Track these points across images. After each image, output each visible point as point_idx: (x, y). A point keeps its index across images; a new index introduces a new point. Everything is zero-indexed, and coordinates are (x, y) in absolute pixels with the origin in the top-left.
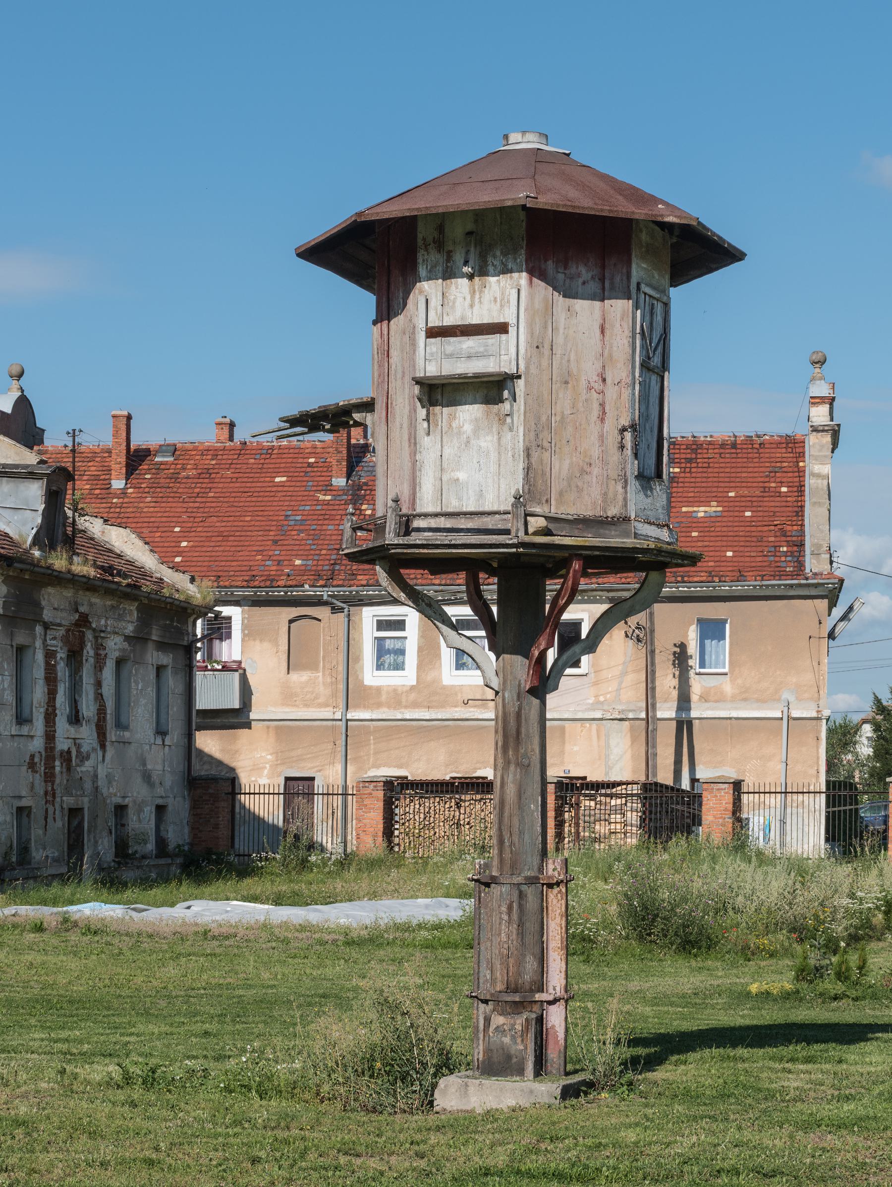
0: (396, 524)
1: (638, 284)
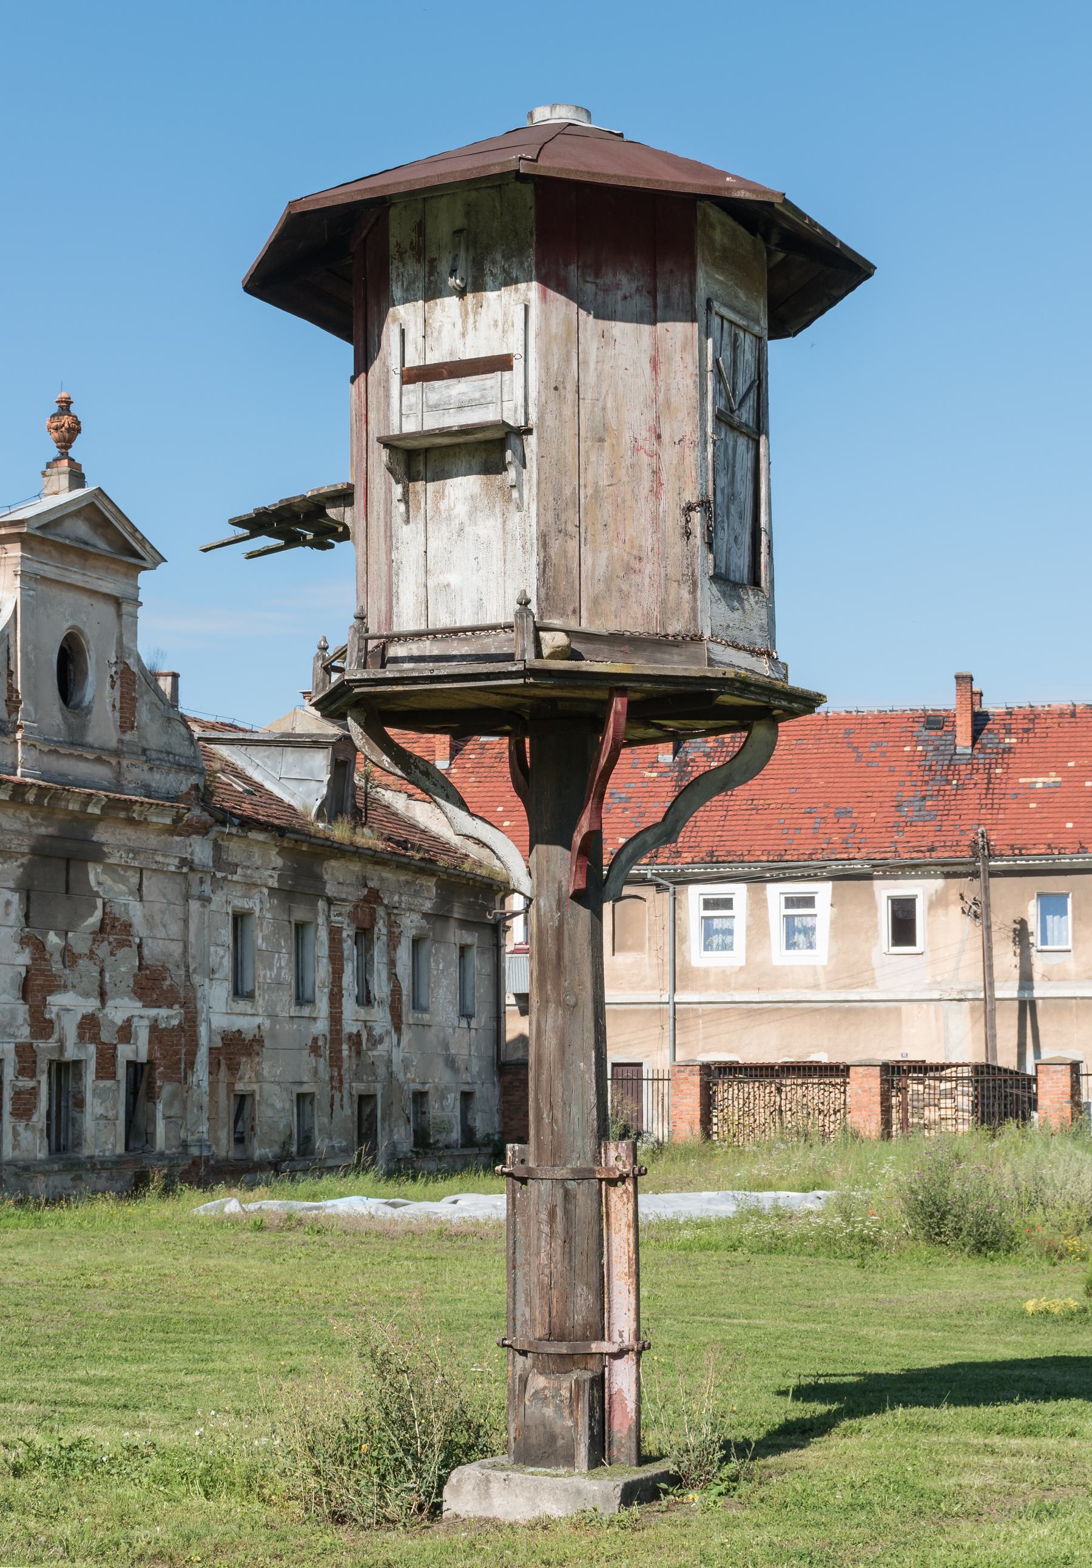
0: (360, 650)
1: (709, 301)
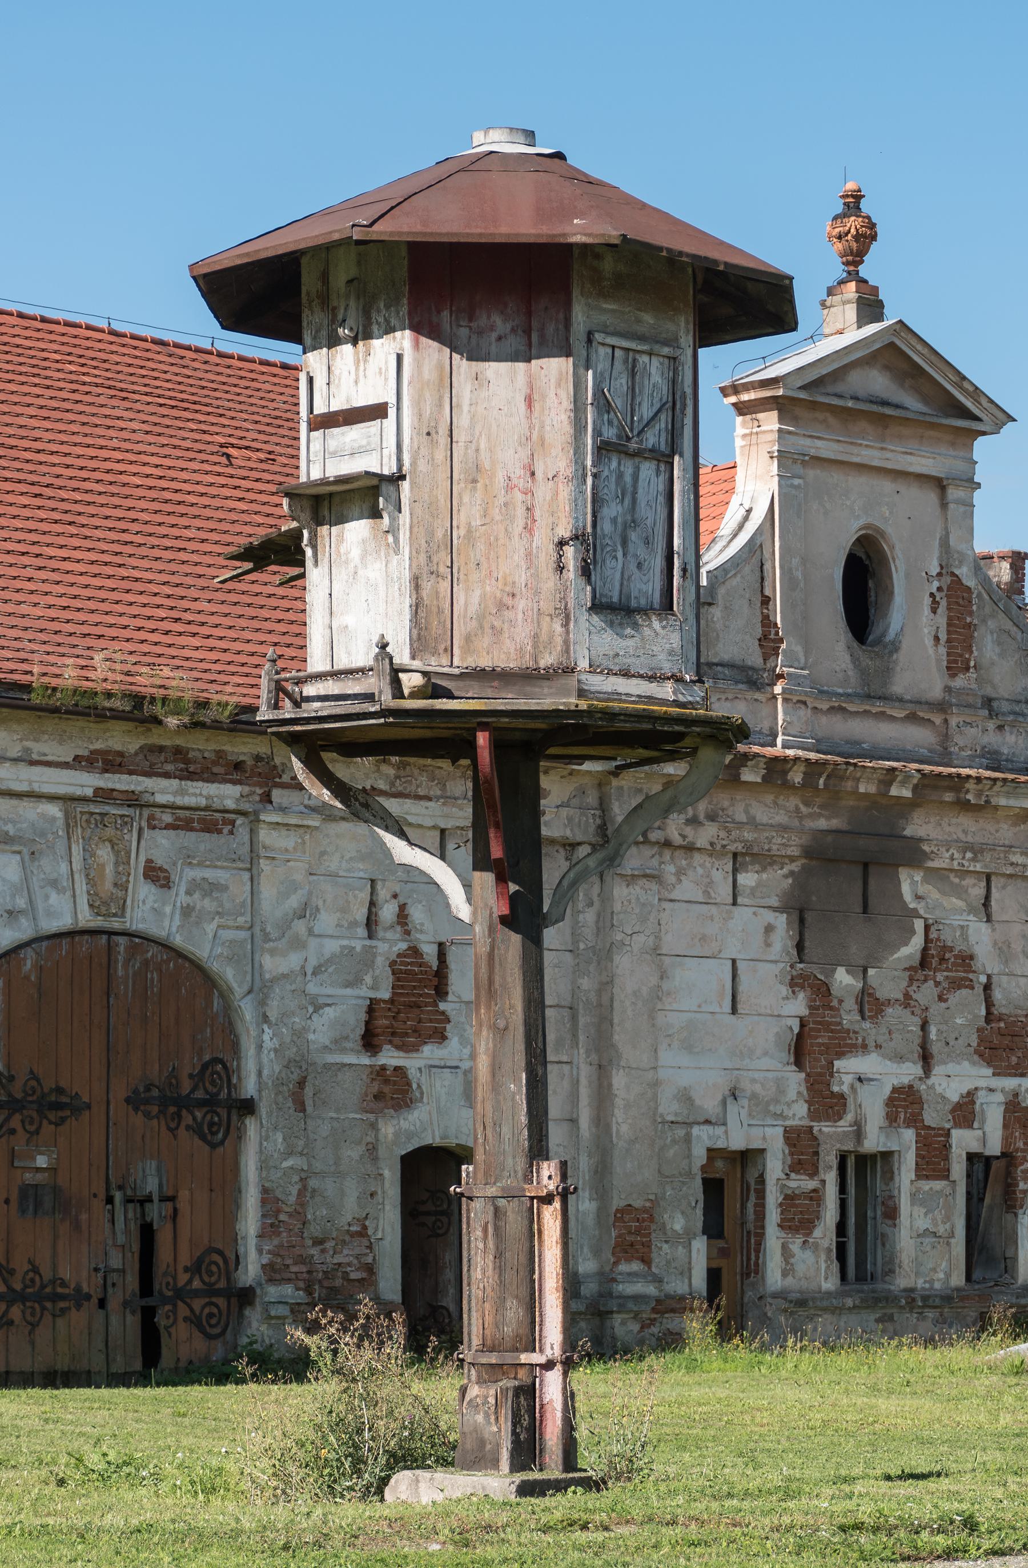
1: (590, 335)
